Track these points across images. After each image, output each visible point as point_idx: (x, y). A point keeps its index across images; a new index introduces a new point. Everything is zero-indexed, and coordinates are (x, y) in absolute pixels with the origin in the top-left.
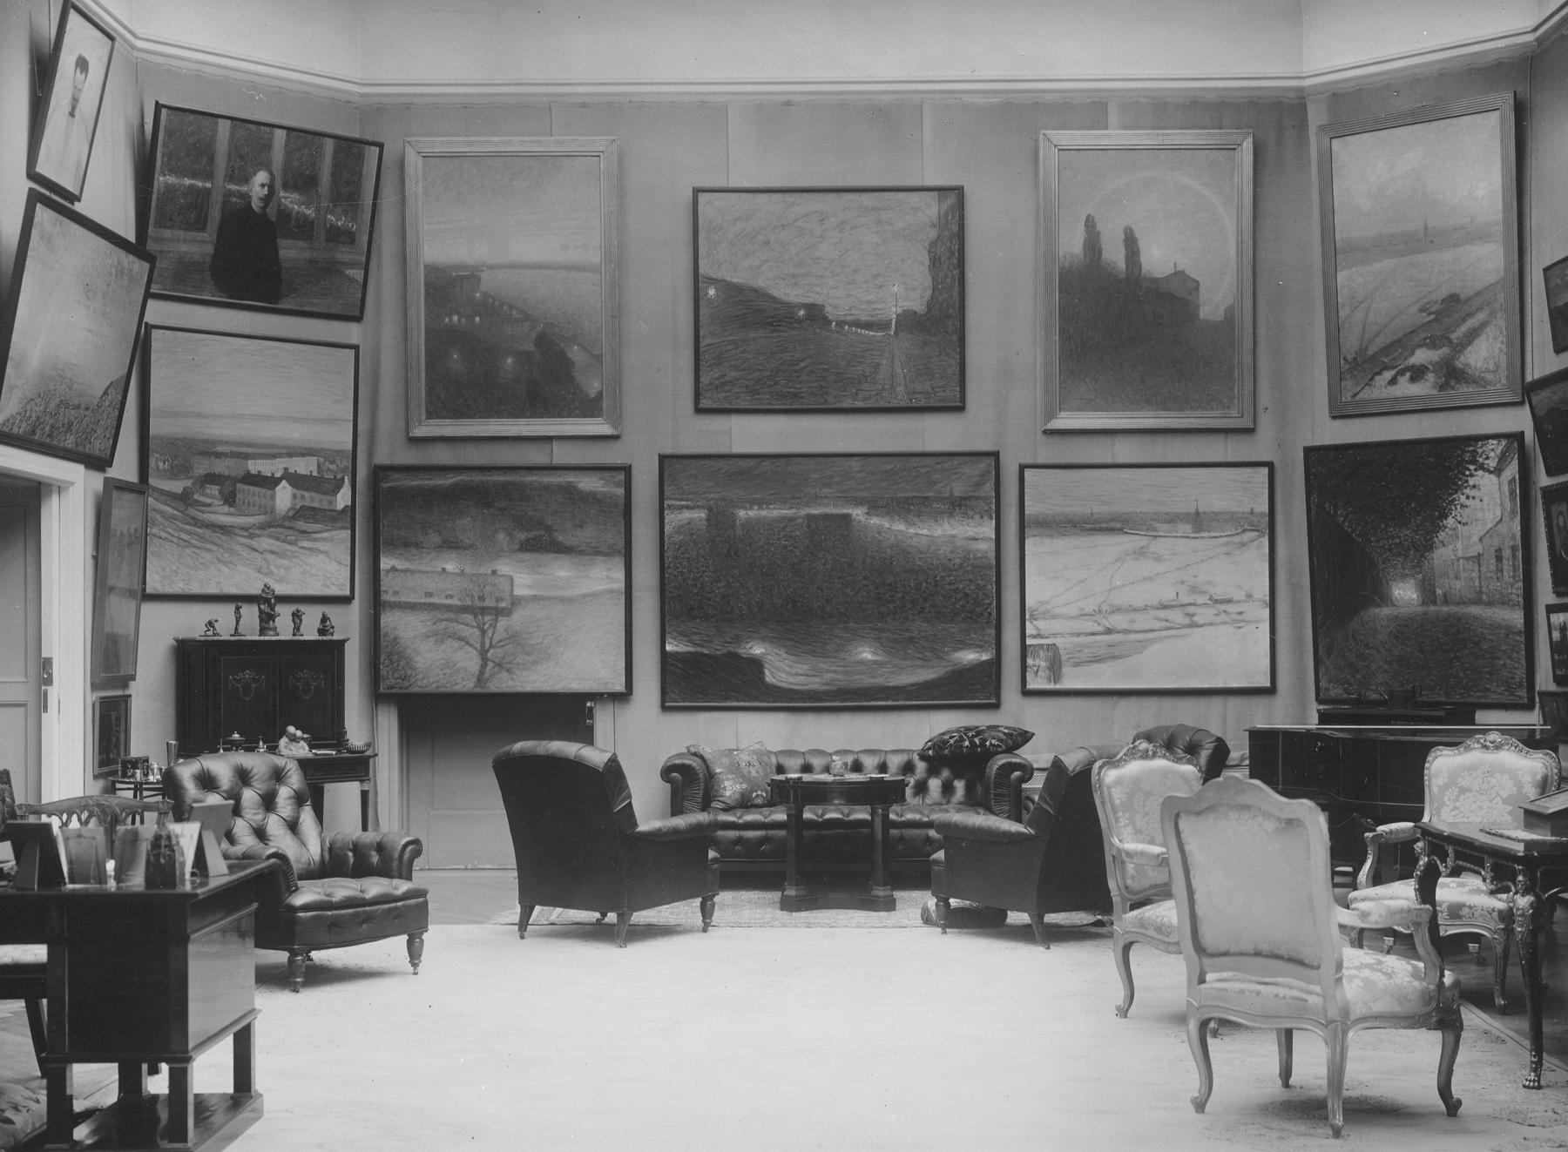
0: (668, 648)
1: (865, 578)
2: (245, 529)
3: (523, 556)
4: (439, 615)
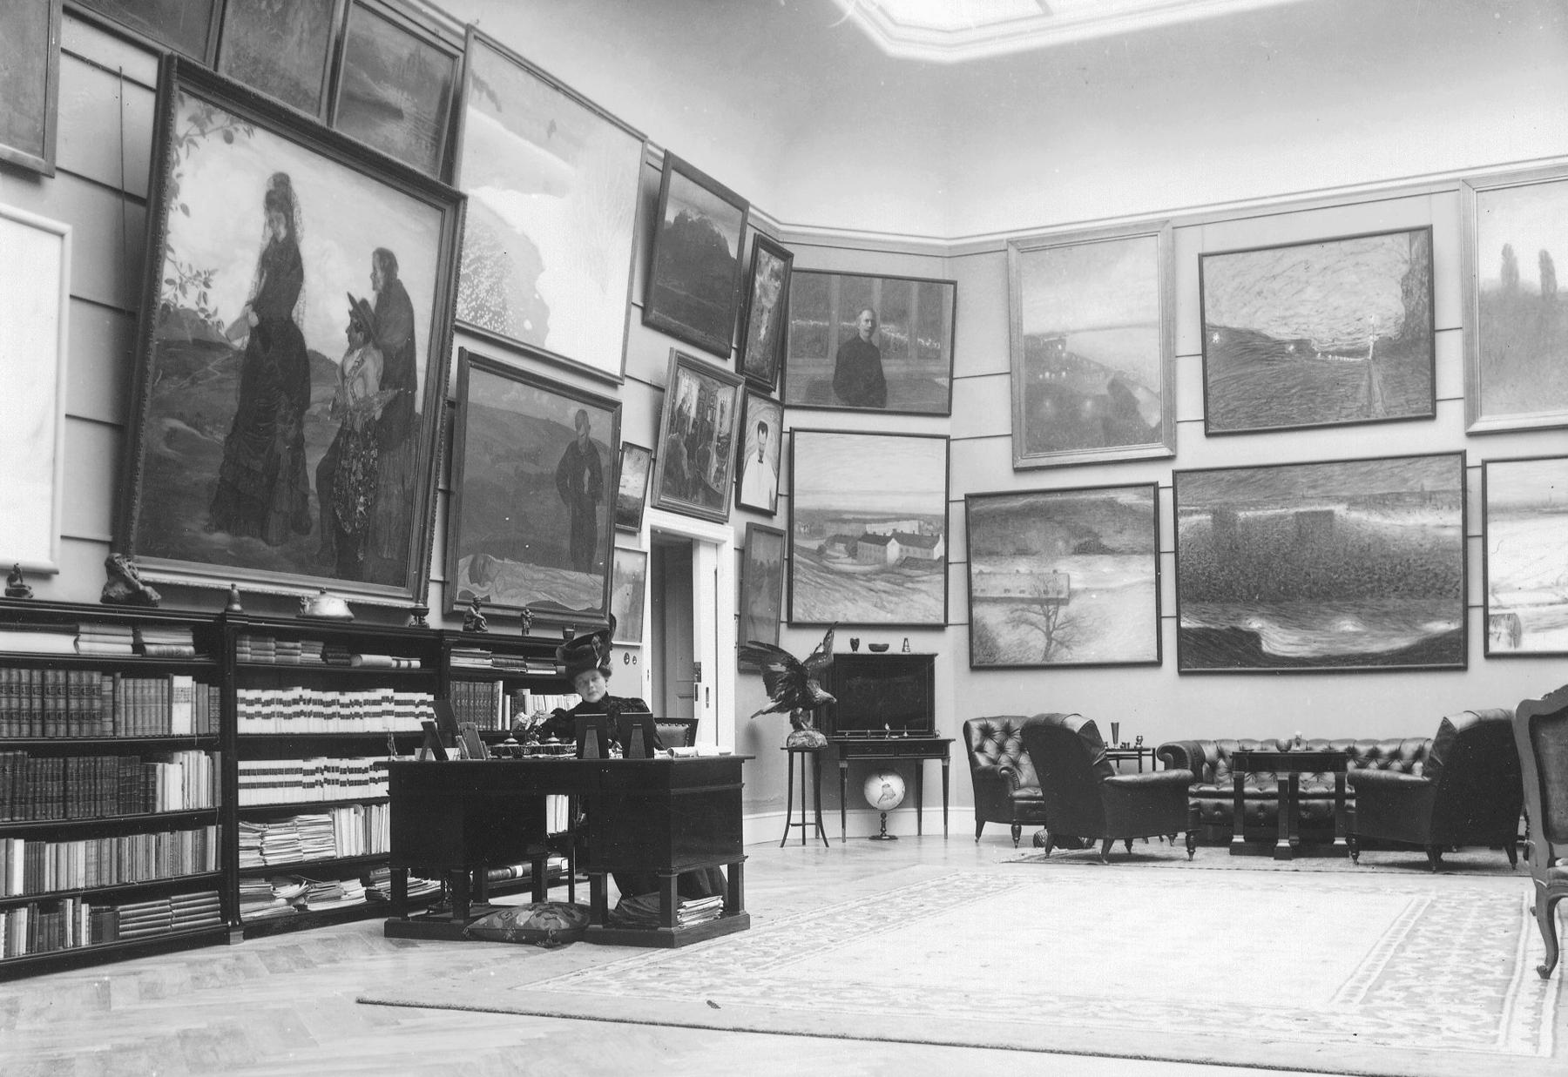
0: (1183, 625)
1: (1346, 563)
2: (865, 574)
3: (1077, 558)
4: (1014, 606)
